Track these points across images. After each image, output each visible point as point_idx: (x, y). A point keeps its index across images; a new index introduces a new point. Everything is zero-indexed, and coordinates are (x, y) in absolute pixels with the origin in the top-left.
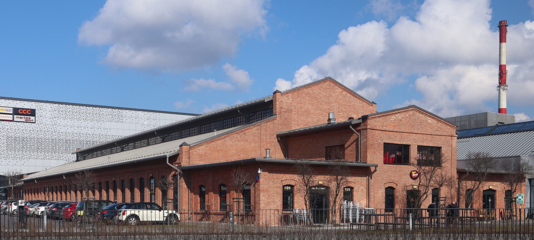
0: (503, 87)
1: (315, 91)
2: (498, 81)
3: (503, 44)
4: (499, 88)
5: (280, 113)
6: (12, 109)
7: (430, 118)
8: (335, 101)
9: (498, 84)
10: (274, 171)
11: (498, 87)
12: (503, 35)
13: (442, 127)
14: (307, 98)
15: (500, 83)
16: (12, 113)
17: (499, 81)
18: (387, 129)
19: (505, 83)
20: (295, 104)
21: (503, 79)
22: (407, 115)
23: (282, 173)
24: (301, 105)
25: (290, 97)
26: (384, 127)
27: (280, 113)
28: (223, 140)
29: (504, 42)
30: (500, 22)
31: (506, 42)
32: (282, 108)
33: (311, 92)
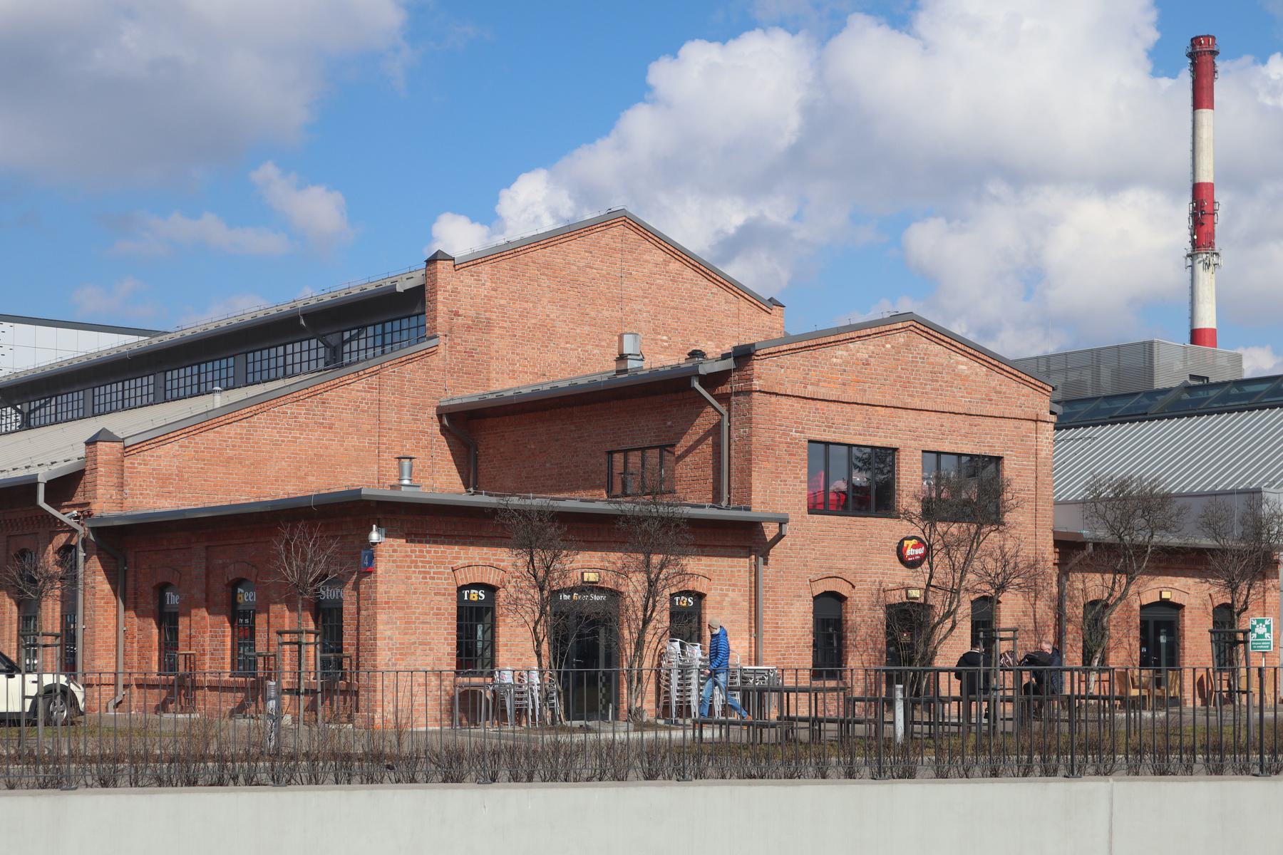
0: (1204, 256)
1: (571, 258)
2: (1189, 238)
4: (1193, 260)
5: (451, 331)
7: (965, 359)
8: (640, 293)
9: (1189, 246)
10: (425, 535)
11: (1189, 256)
12: (1205, 82)
13: (1004, 389)
14: (545, 281)
15: (1195, 244)
17: (1192, 235)
18: (822, 392)
19: (1211, 244)
20: (503, 302)
21: (1205, 229)
22: (888, 346)
23: (457, 543)
24: (525, 305)
25: (484, 277)
26: (810, 388)
27: (451, 331)
28: (244, 423)
29: (1207, 108)
30: (1195, 41)
31: (1212, 108)
32: (457, 314)
33: (559, 260)
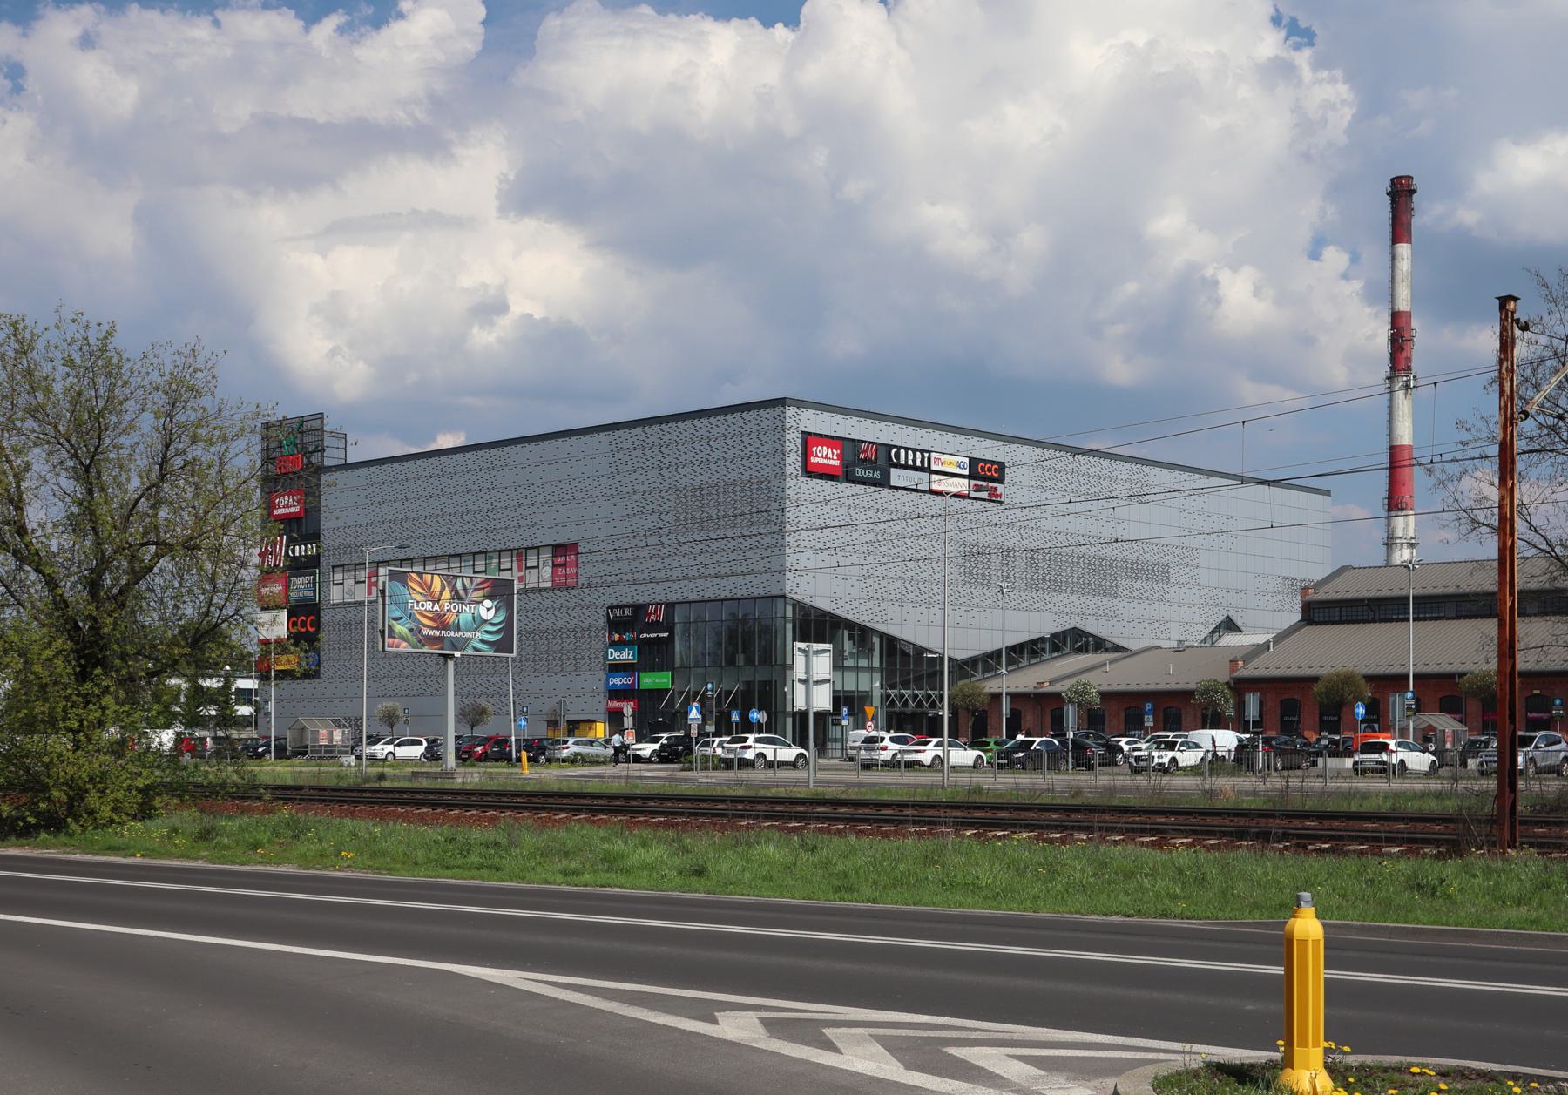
3: (1404, 249)
6: (967, 460)
11: (1388, 378)
15: (1393, 369)
16: (966, 472)
